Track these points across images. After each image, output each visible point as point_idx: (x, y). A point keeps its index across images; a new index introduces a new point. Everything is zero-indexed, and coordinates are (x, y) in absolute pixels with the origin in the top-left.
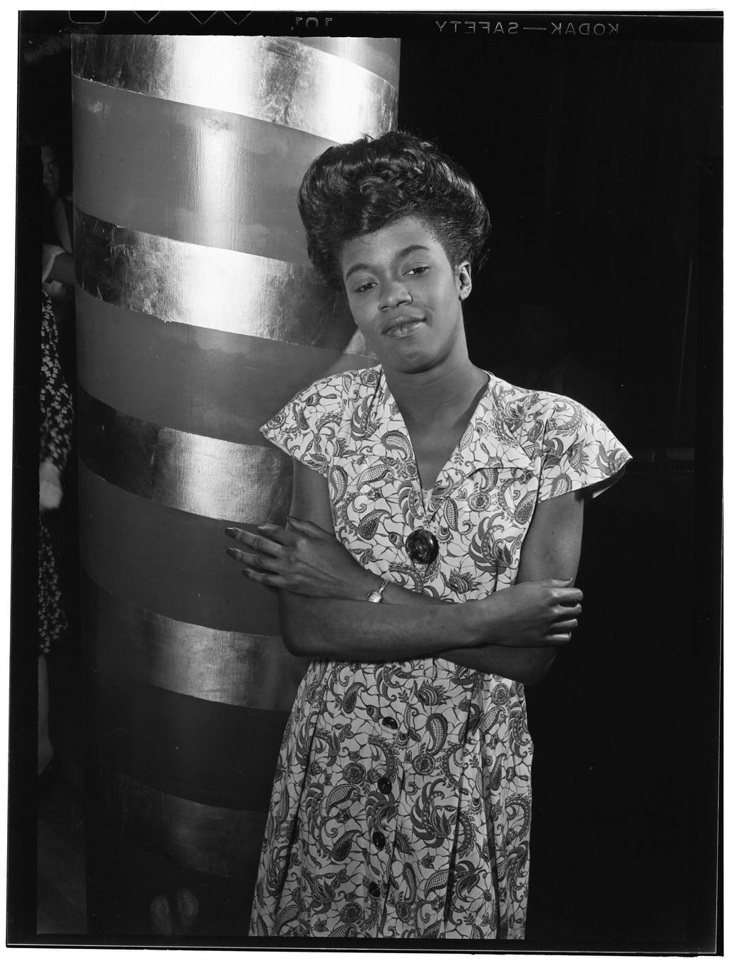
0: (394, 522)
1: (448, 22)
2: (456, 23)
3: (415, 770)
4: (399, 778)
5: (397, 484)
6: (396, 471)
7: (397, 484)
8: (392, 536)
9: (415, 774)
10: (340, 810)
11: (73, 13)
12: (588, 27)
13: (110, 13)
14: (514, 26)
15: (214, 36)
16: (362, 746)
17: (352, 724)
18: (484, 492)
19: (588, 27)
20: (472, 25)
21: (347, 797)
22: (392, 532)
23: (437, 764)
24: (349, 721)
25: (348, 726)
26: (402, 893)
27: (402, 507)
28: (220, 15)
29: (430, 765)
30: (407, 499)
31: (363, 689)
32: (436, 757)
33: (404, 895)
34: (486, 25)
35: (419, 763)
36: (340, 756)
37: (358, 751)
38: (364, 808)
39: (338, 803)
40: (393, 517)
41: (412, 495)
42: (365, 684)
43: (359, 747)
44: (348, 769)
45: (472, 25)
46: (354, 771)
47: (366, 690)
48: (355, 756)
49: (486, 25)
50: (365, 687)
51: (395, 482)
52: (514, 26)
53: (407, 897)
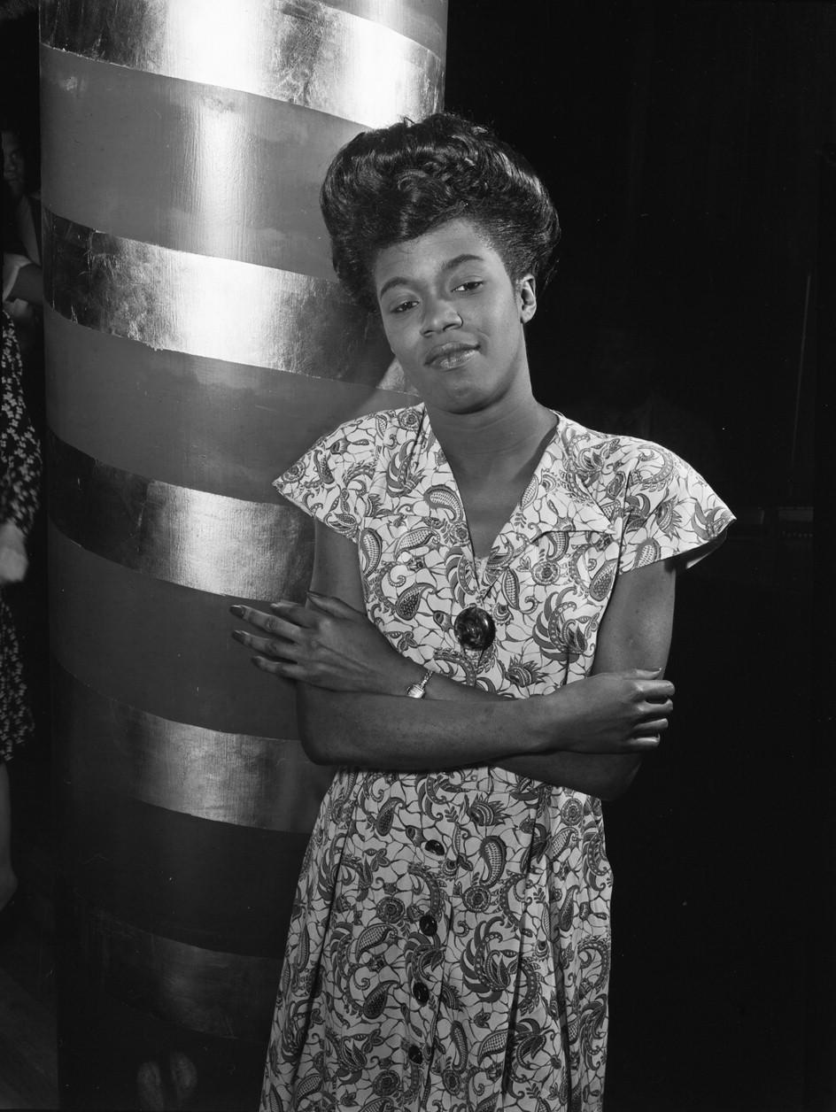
0: (440, 598)
3: (465, 905)
4: (446, 916)
5: (444, 551)
6: (442, 535)
7: (444, 551)
8: (438, 615)
9: (465, 911)
10: (373, 956)
16: (400, 877)
17: (388, 848)
21: (382, 940)
22: (437, 611)
23: (493, 899)
24: (384, 846)
25: (383, 852)
26: (450, 1058)
27: (450, 579)
29: (485, 899)
30: (456, 570)
31: (401, 805)
32: (492, 890)
33: (452, 1061)
35: (471, 898)
36: (373, 889)
37: (396, 883)
39: (370, 947)
40: (439, 591)
41: (462, 564)
42: (404, 799)
43: (396, 877)
44: (383, 904)
46: (390, 907)
47: (406, 807)
48: (391, 888)
50: (404, 803)
51: (441, 548)
53: (456, 1063)
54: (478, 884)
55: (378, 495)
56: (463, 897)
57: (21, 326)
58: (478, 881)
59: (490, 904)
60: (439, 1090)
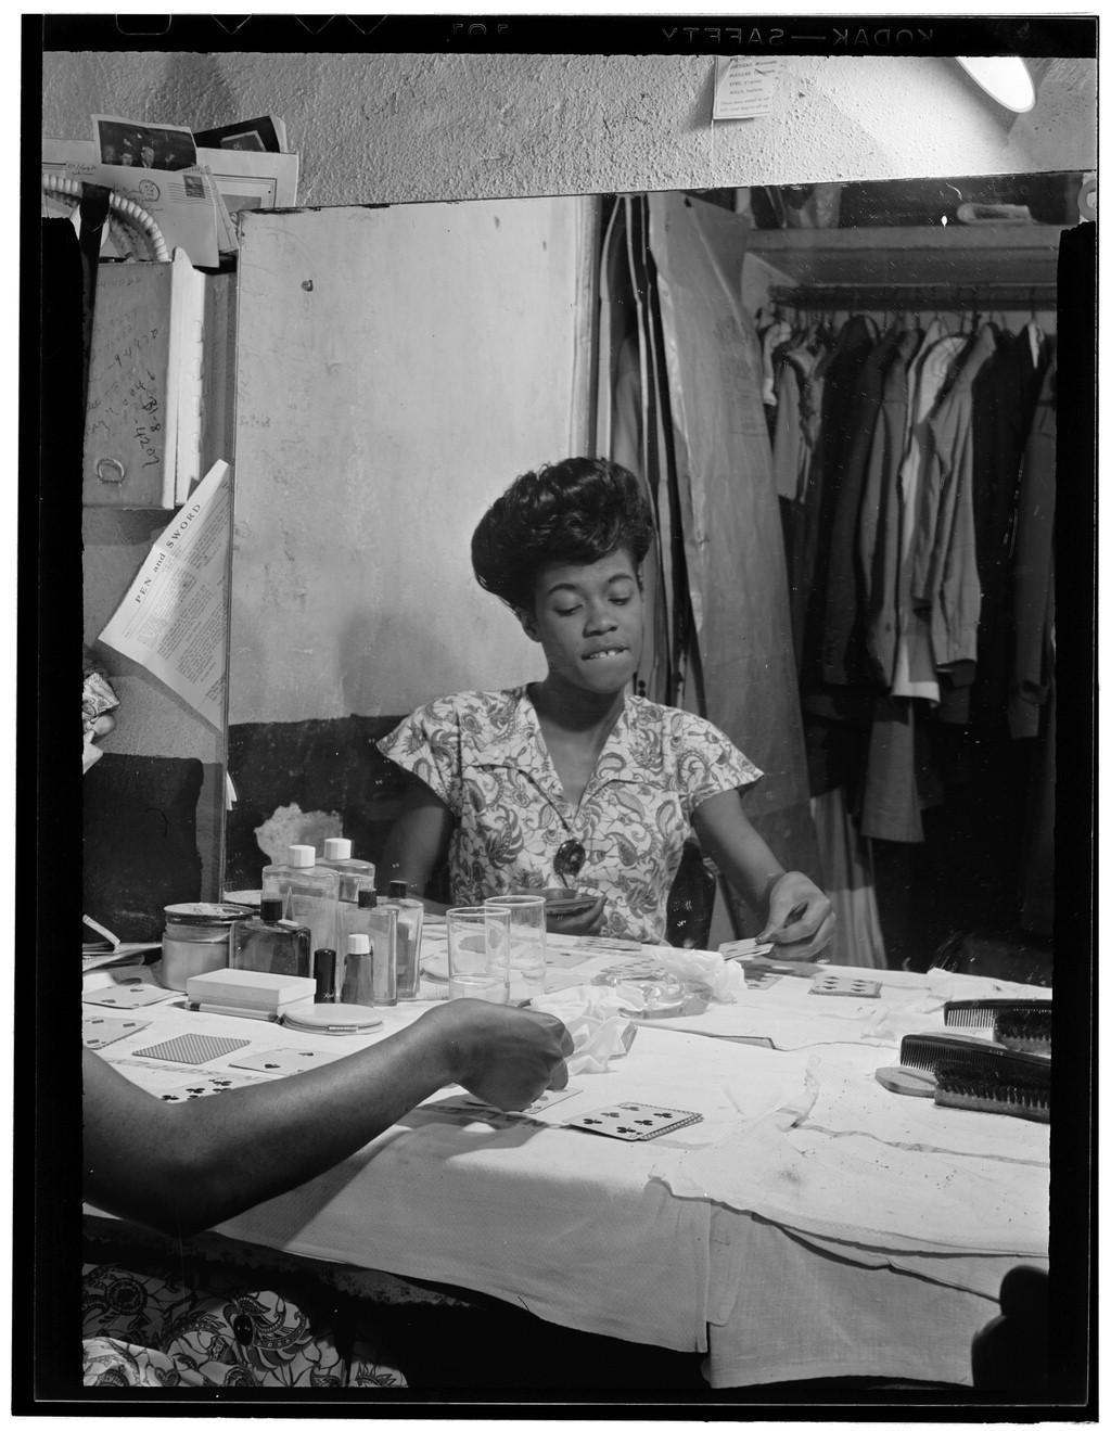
0: (321, 1356)
1: (680, 30)
2: (691, 30)
3: (145, 1301)
4: (191, 1308)
9: (152, 1296)
11: (122, 17)
12: (888, 35)
13: (176, 17)
14: (778, 33)
15: (854, 1373)
18: (107, 1303)
19: (888, 35)
20: (716, 33)
23: (108, 1282)
26: (101, 1321)
27: (292, 1356)
28: (341, 20)
29: (118, 1289)
30: (280, 1351)
32: (101, 1292)
33: (102, 1317)
34: (736, 33)
35: (132, 1303)
38: (270, 1374)
40: (313, 1361)
41: (270, 1345)
42: (308, 1373)
45: (716, 33)
47: (317, 1364)
49: (736, 33)
50: (313, 1368)
52: (778, 33)
53: (99, 1311)
54: (111, 1310)
55: (699, 1116)
56: (140, 1312)
57: (1003, 1031)
58: (108, 1314)
59: (116, 1280)
60: (158, 1301)
